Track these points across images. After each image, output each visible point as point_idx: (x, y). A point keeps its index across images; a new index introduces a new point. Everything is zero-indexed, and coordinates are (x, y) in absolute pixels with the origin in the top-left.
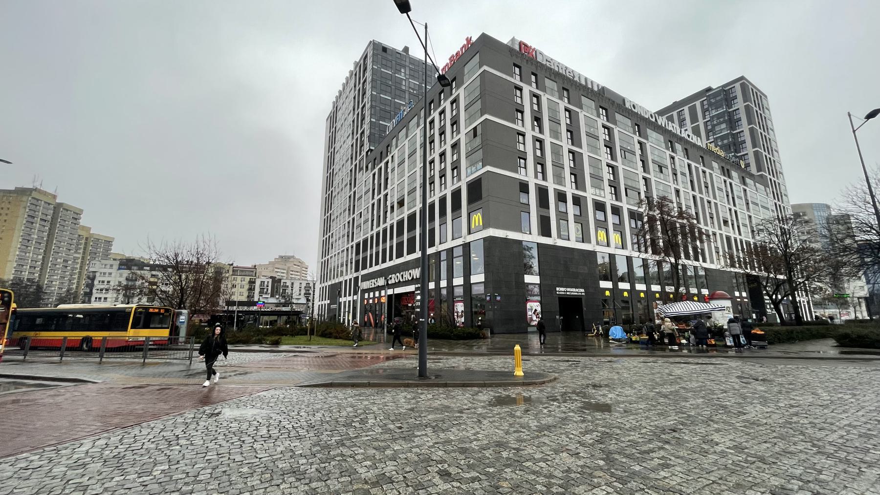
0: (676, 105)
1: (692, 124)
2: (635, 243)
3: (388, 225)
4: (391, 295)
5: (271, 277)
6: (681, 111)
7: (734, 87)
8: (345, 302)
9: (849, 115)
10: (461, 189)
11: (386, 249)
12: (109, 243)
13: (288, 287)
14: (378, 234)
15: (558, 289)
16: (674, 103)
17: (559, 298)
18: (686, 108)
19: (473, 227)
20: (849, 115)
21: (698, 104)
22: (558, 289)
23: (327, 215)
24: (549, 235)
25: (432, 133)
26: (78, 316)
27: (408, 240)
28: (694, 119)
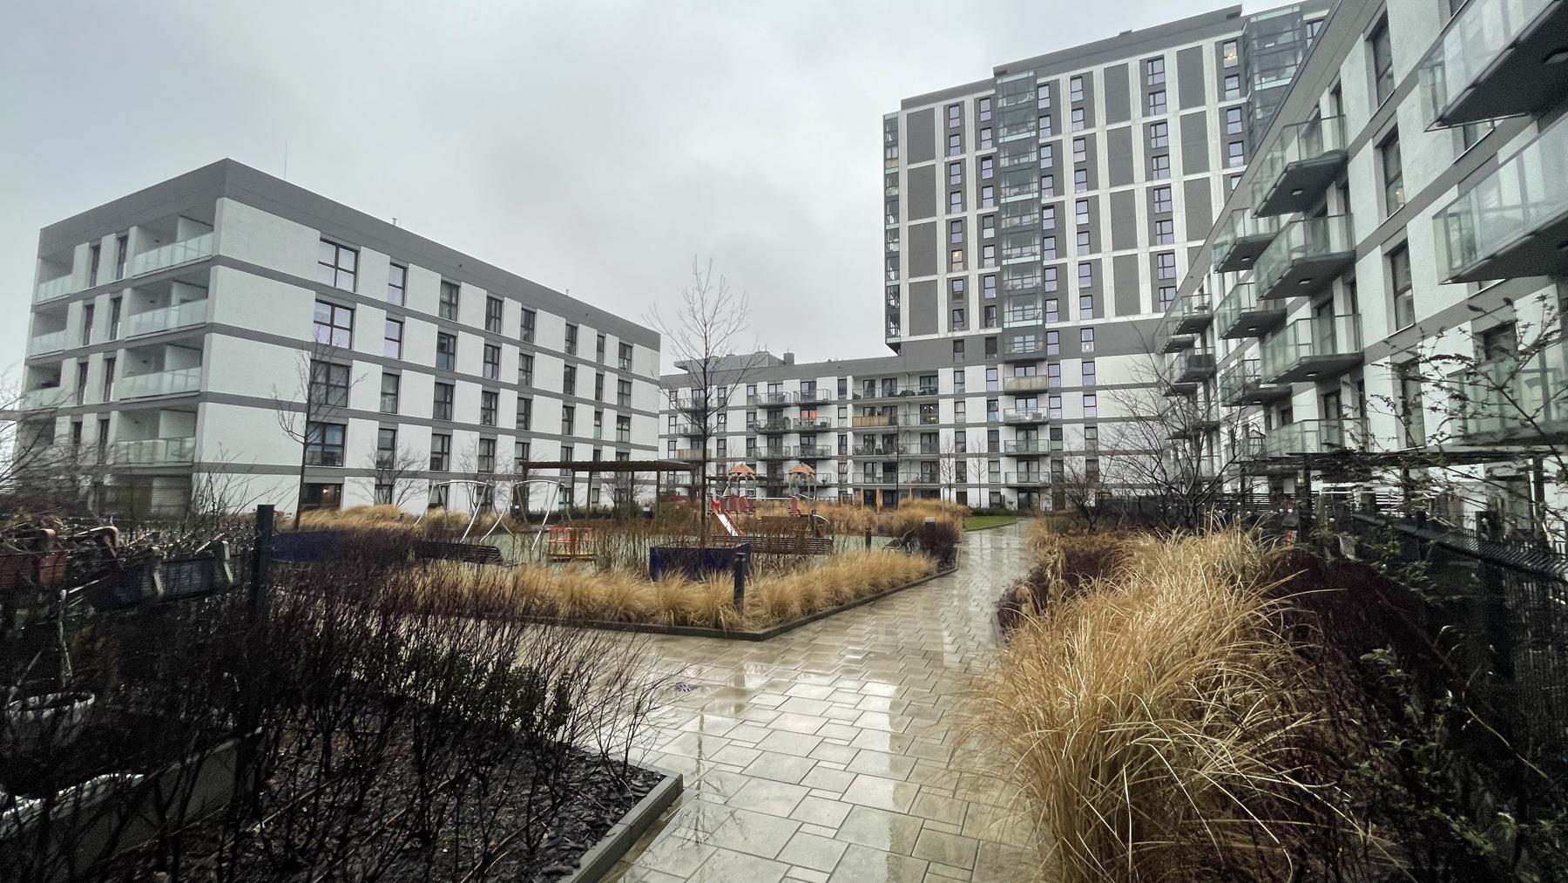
0: (1127, 43)
1: (1182, 108)
2: (597, 453)
6: (1151, 60)
7: (1161, 58)
9: (711, 260)
12: (789, 358)
16: (1122, 34)
18: (1170, 55)
20: (711, 260)
21: (1208, 46)
26: (1295, 193)
28: (1192, 92)
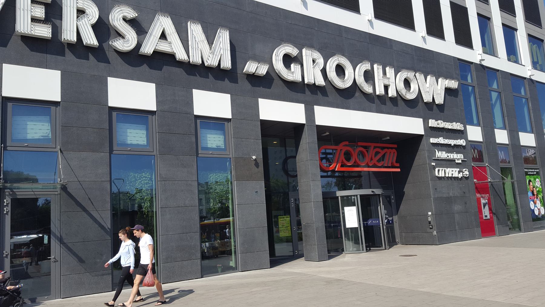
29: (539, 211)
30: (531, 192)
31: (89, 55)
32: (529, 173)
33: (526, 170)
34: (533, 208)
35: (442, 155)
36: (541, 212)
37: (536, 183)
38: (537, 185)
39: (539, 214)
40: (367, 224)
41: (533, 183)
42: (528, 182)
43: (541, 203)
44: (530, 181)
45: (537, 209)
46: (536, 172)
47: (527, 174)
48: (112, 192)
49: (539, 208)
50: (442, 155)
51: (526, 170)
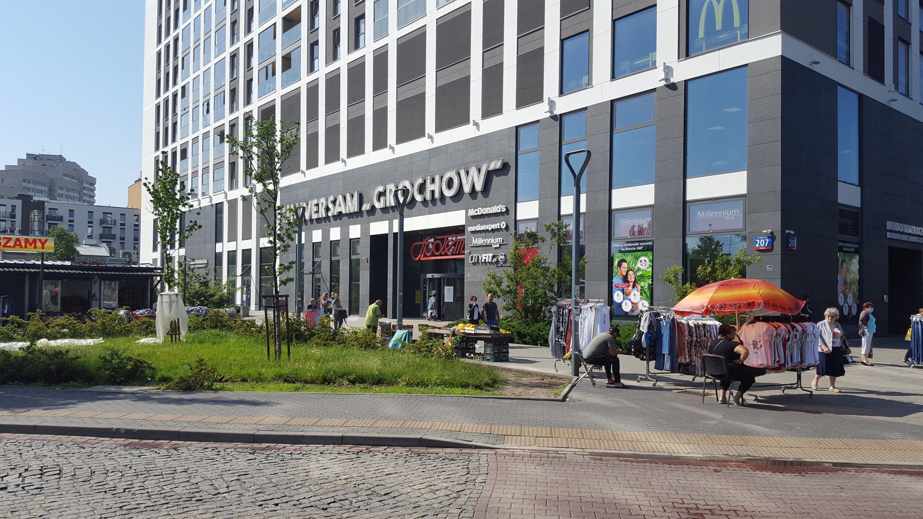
3: (368, 50)
4: (384, 237)
5: (20, 197)
8: (232, 255)
10: (425, 33)
11: (337, 127)
13: (61, 219)
14: (333, 81)
15: (889, 225)
17: (892, 250)
19: (701, 34)
22: (889, 225)
23: (164, 42)
24: (880, 78)
25: (236, 8)
27: (349, 121)
29: (849, 311)
30: (622, 277)
31: (141, 187)
32: (844, 249)
33: (841, 244)
34: (841, 304)
35: (479, 241)
36: (853, 311)
37: (852, 265)
38: (853, 269)
39: (848, 314)
40: (633, 352)
41: (847, 265)
42: (840, 262)
43: (853, 298)
44: (843, 261)
45: (847, 307)
46: (854, 249)
47: (840, 249)
48: (489, 295)
49: (850, 304)
50: (479, 241)
51: (841, 244)
